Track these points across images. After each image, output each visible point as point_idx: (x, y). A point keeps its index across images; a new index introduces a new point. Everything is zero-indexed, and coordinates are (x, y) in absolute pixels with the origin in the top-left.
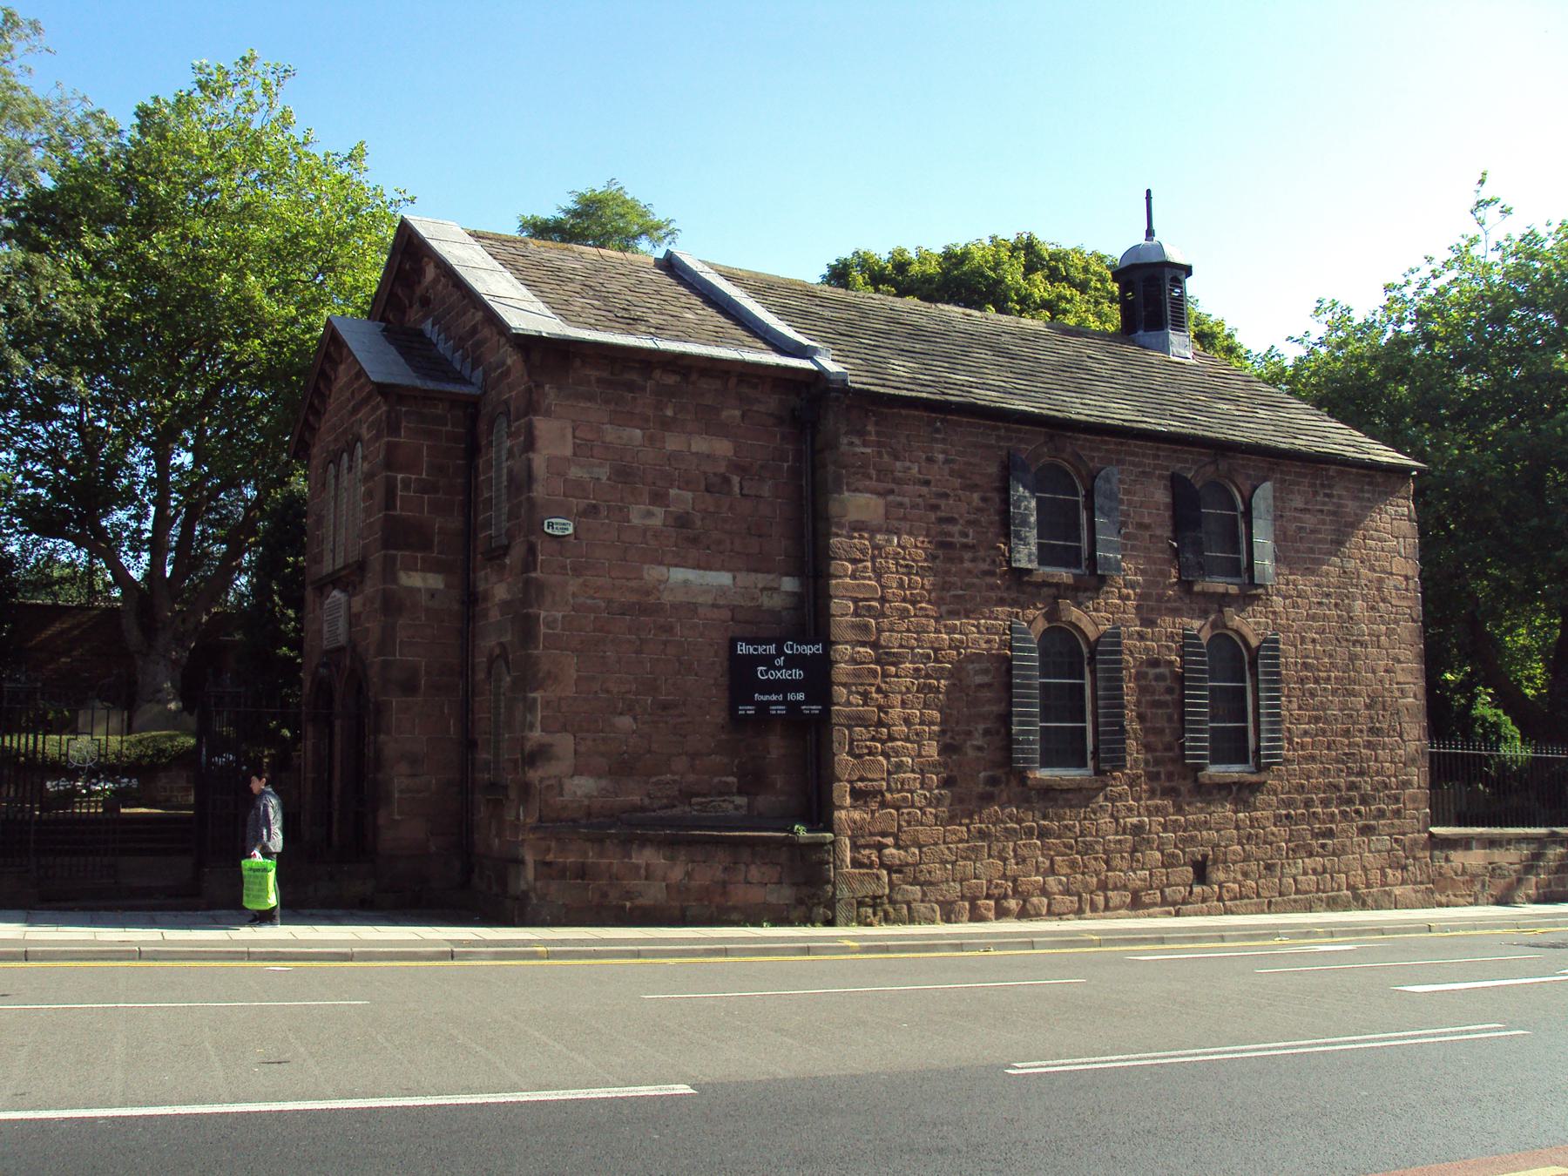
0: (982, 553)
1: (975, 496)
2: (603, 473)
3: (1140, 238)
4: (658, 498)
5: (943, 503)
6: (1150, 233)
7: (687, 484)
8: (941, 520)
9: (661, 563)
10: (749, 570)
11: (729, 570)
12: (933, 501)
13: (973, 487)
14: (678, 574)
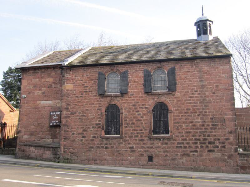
0: (93, 92)
1: (93, 81)
2: (31, 87)
3: (200, 16)
4: (40, 90)
5: (85, 84)
6: (203, 15)
7: (45, 87)
8: (85, 87)
9: (40, 100)
10: (54, 100)
11: (51, 100)
12: (83, 84)
13: (93, 80)
14: (43, 102)
